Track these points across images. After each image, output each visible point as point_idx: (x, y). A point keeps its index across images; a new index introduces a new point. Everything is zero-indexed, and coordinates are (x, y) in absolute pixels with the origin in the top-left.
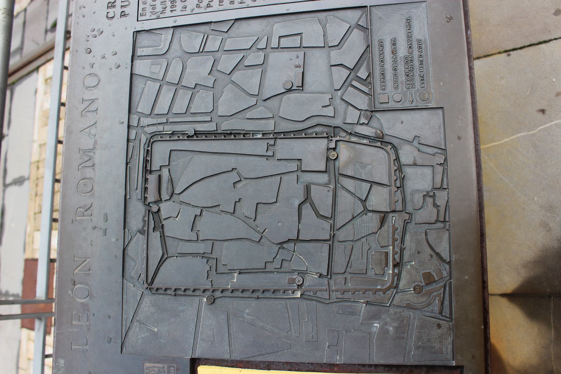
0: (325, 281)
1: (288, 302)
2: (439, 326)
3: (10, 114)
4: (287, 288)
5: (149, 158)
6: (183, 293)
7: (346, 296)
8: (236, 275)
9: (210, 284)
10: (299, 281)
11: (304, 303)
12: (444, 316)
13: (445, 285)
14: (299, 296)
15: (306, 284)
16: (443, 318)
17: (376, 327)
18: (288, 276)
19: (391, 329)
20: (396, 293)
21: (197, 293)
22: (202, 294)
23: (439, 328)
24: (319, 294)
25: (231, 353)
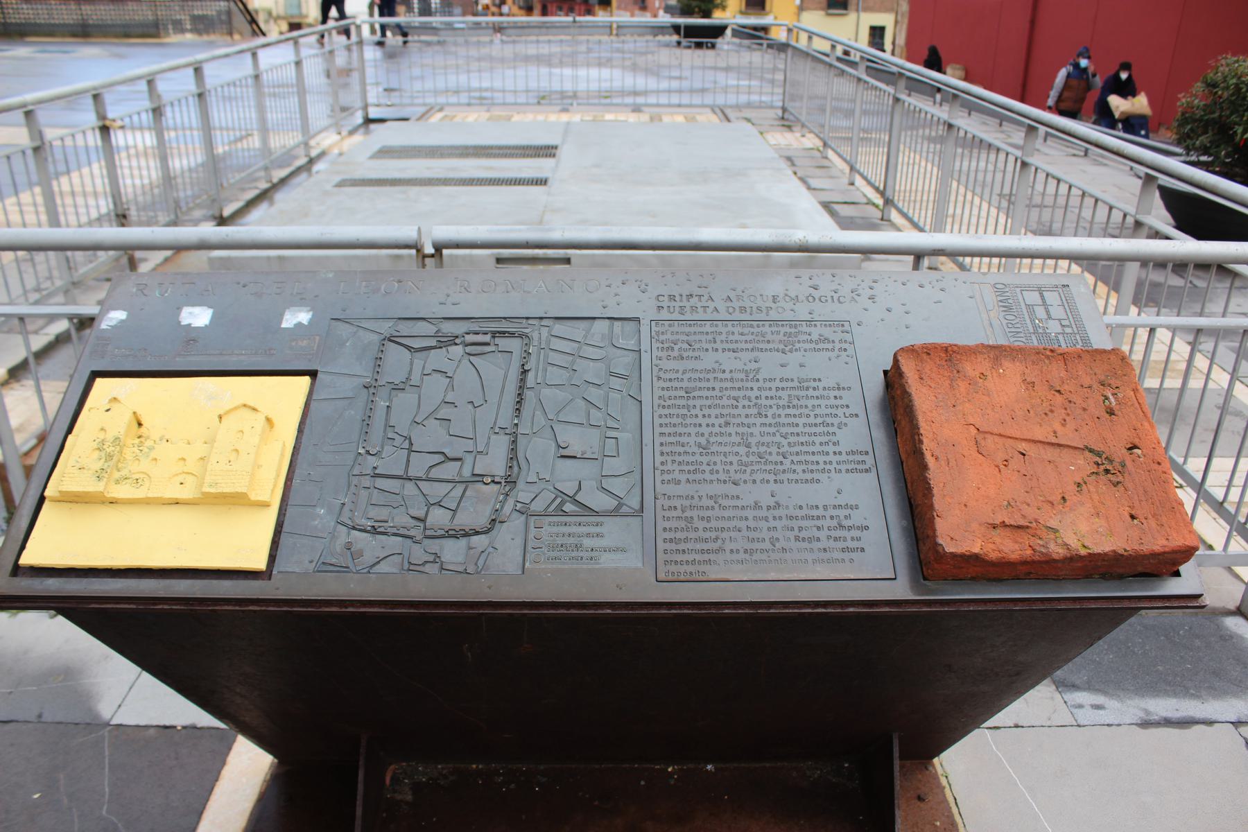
11: (352, 456)
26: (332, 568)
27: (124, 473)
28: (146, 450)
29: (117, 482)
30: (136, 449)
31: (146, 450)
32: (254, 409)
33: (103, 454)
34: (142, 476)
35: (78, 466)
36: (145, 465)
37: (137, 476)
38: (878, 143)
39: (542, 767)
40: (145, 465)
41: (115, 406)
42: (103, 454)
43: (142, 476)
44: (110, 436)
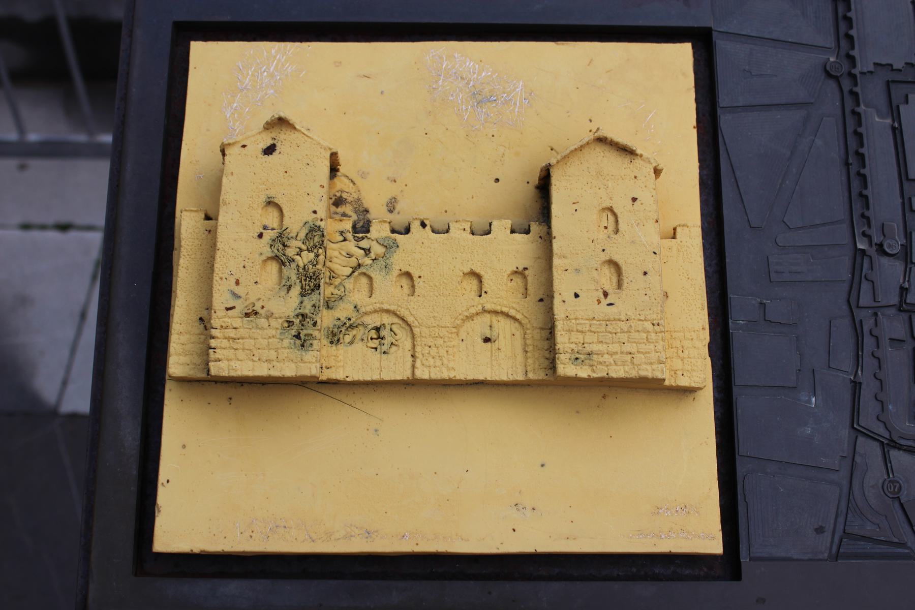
0: (895, 300)
1: (845, 226)
2: (820, 530)
3: (858, 412)
4: (873, 223)
5: (896, 125)
6: (840, 14)
7: (869, 342)
8: (889, 121)
9: (865, 70)
10: (890, 246)
11: (847, 261)
12: (841, 541)
13: (903, 545)
14: (860, 246)
15: (885, 261)
16: (836, 540)
17: (809, 401)
18: (896, 226)
19: (809, 431)
20: (882, 443)
21: (844, 43)
22: (843, 53)
23: (816, 530)
24: (865, 286)
25: (733, 109)
26: (868, 547)
27: (343, 311)
28: (377, 249)
29: (334, 338)
30: (351, 246)
31: (377, 249)
32: (626, 151)
33: (291, 272)
34: (387, 319)
35: (240, 306)
36: (389, 291)
37: (374, 320)
38: (93, 151)
39: (687, 572)
40: (389, 291)
41: (284, 138)
42: (291, 272)
43: (387, 319)
44: (295, 222)
